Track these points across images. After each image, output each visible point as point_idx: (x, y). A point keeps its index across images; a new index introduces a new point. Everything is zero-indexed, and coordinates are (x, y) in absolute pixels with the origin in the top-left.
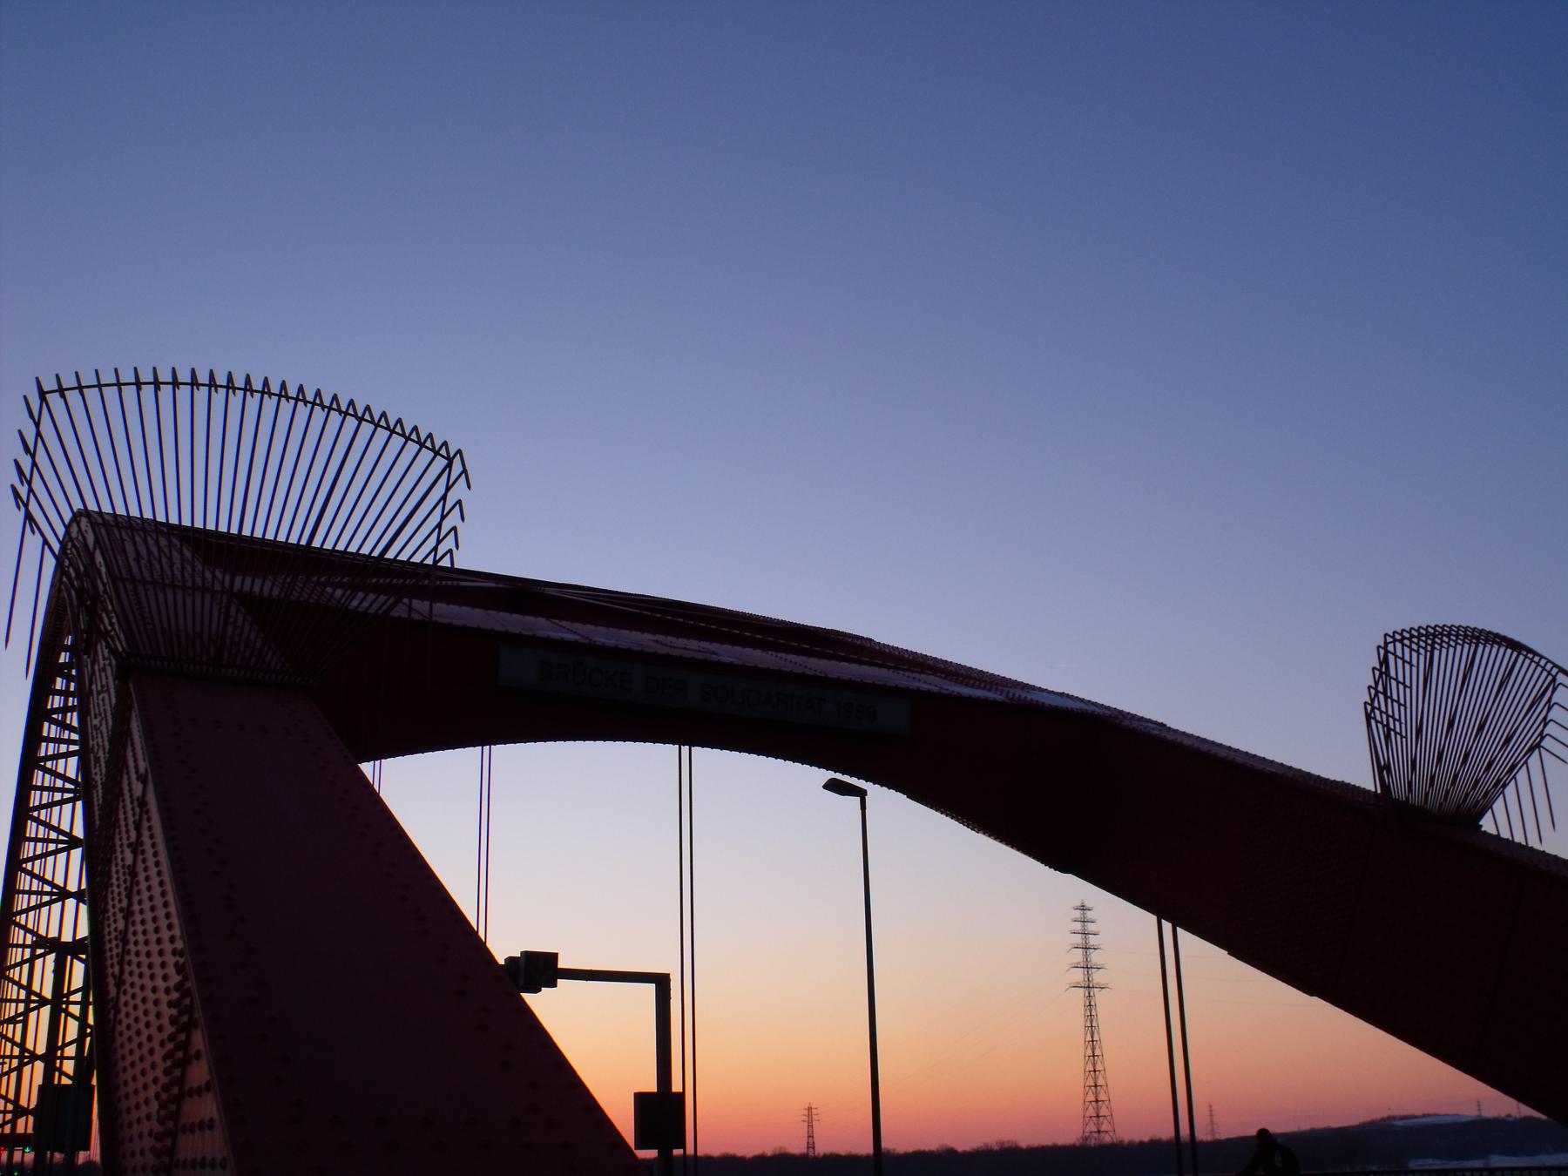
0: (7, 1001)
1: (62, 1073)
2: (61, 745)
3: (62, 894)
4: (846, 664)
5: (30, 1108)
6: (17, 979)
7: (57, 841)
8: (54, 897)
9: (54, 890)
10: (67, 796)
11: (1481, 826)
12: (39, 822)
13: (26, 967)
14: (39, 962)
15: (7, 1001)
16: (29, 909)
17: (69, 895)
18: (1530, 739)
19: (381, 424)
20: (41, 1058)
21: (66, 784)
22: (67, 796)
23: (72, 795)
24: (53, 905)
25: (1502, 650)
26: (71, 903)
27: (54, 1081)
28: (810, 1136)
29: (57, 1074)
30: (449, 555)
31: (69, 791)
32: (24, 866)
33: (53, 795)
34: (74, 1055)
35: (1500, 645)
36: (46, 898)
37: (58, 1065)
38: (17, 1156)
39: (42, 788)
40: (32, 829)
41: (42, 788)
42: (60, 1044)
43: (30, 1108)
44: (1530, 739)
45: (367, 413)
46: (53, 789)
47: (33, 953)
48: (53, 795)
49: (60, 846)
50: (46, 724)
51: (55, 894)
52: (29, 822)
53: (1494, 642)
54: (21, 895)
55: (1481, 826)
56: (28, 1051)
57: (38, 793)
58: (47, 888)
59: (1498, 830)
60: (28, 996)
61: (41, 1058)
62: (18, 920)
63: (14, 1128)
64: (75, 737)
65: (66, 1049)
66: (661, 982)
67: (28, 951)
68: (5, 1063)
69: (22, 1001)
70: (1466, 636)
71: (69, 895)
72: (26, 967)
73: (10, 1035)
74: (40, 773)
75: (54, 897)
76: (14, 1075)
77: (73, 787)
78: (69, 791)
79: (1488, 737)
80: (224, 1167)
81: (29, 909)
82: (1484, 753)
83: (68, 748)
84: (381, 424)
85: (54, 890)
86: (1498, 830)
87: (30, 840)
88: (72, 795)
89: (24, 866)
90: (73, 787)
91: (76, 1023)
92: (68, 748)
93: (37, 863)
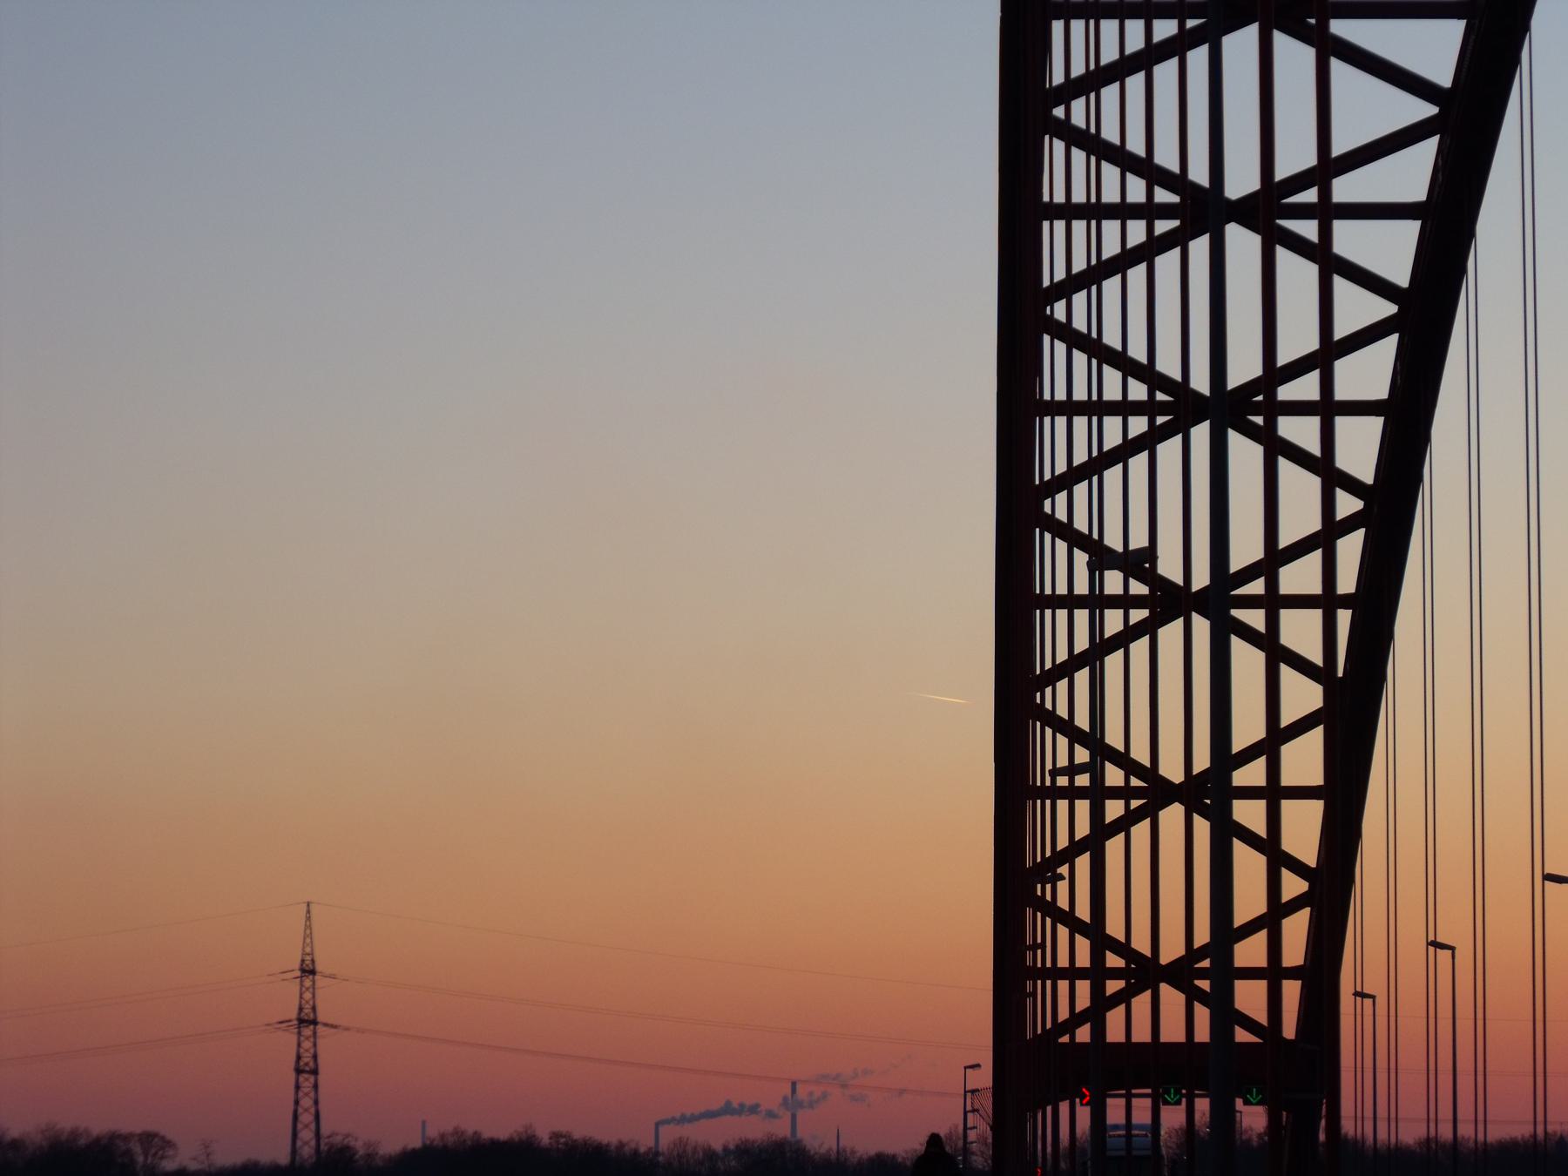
0: (1056, 974)
5: (1194, 589)
8: (1191, 23)
9: (1160, 396)
10: (1162, 226)
13: (1082, 677)
14: (1114, 846)
15: (1056, 974)
22: (1162, 226)
23: (1175, 223)
31: (1166, 211)
32: (1059, 112)
38: (1115, 1110)
43: (1194, 589)
47: (1097, 991)
51: (1163, 408)
52: (1047, 339)
57: (1060, 225)
59: (1543, 883)
60: (1097, 955)
62: (1061, 515)
63: (1099, 1030)
66: (965, 1068)
67: (1083, 988)
68: (1061, 878)
69: (1082, 974)
72: (1082, 677)
73: (1062, 711)
77: (1175, 199)
78: (1166, 211)
85: (1160, 396)
86: (1543, 883)
87: (1055, 408)
88: (1175, 223)
90: (1175, 199)
93: (1079, 299)
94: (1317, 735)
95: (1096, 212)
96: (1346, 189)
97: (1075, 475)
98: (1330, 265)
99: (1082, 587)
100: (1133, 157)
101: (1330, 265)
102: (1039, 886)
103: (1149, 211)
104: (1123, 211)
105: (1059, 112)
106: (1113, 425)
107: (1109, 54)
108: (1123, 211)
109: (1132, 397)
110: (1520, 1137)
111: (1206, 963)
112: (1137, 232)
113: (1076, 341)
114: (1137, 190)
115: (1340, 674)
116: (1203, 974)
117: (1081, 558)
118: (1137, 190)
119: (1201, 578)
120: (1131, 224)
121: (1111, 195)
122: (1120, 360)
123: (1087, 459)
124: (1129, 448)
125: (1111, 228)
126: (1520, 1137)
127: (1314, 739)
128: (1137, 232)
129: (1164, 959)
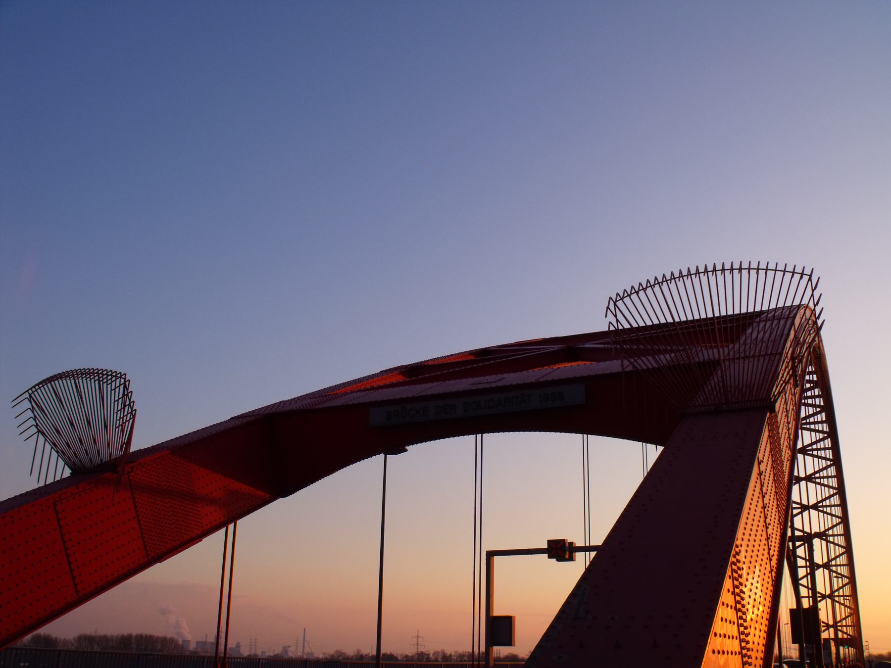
1: (807, 587)
2: (810, 395)
3: (809, 478)
4: (386, 389)
5: (810, 505)
6: (834, 518)
7: (812, 450)
8: (814, 476)
10: (821, 504)
11: (70, 473)
12: (822, 432)
13: (844, 584)
16: (839, 556)
17: (802, 479)
18: (49, 425)
19: (620, 298)
20: (819, 566)
21: (819, 482)
22: (821, 504)
23: (819, 505)
24: (813, 472)
25: (45, 386)
26: (802, 475)
27: (808, 545)
28: (372, 650)
29: (807, 558)
30: (611, 300)
31: (820, 507)
32: (832, 463)
33: (814, 420)
34: (799, 569)
35: (57, 379)
36: (817, 475)
37: (808, 563)
39: (825, 449)
40: (833, 482)
41: (825, 449)
42: (809, 576)
43: (810, 505)
44: (49, 425)
45: (625, 296)
46: (817, 450)
48: (814, 420)
49: (810, 448)
50: (822, 404)
52: (836, 487)
53: (66, 377)
54: (833, 475)
55: (70, 473)
56: (824, 540)
58: (818, 480)
61: (819, 566)
62: (843, 549)
64: (840, 628)
65: (805, 574)
70: (78, 374)
71: (802, 479)
74: (825, 430)
75: (814, 476)
76: (838, 619)
77: (819, 508)
78: (820, 507)
79: (72, 405)
80: (723, 604)
81: (839, 556)
82: (72, 434)
83: (820, 475)
84: (620, 298)
88: (819, 505)
89: (832, 463)
90: (819, 508)
91: (796, 526)
92: (820, 475)
94: (800, 577)
95: (828, 477)
96: (800, 510)
97: (844, 586)
98: (803, 531)
99: (846, 601)
100: (823, 486)
101: (803, 531)
102: (813, 370)
103: (823, 506)
104: (826, 506)
105: (840, 520)
106: (828, 503)
107: (822, 443)
108: (826, 506)
109: (814, 425)
110: (431, 653)
111: (819, 599)
112: (824, 503)
113: (832, 487)
114: (825, 509)
115: (791, 548)
116: (823, 626)
117: (846, 604)
118: (825, 509)
119: (828, 592)
120: (813, 421)
121: (826, 480)
122: (828, 514)
123: (799, 304)
124: (837, 590)
125: (825, 475)
126: (431, 653)
127: (800, 576)
128: (824, 503)
129: (827, 594)
